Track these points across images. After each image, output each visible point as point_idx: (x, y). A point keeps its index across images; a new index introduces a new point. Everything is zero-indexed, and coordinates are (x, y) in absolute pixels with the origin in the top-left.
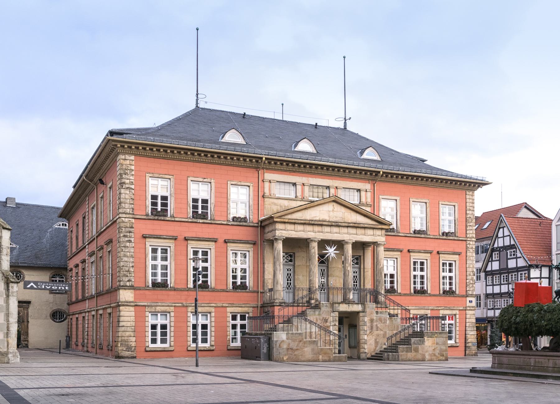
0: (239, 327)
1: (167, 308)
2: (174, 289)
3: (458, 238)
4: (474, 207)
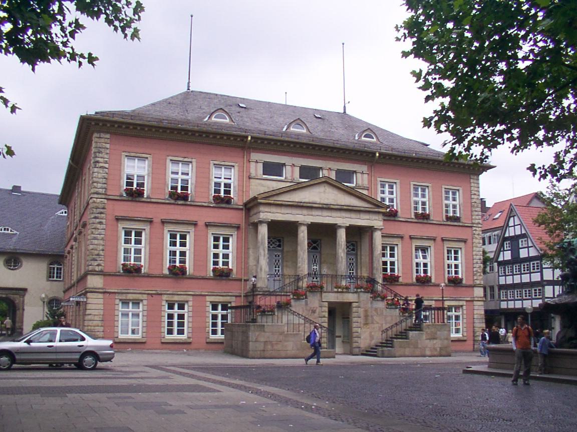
0: (176, 317)
1: (140, 295)
2: (148, 276)
3: (463, 224)
4: (479, 191)
